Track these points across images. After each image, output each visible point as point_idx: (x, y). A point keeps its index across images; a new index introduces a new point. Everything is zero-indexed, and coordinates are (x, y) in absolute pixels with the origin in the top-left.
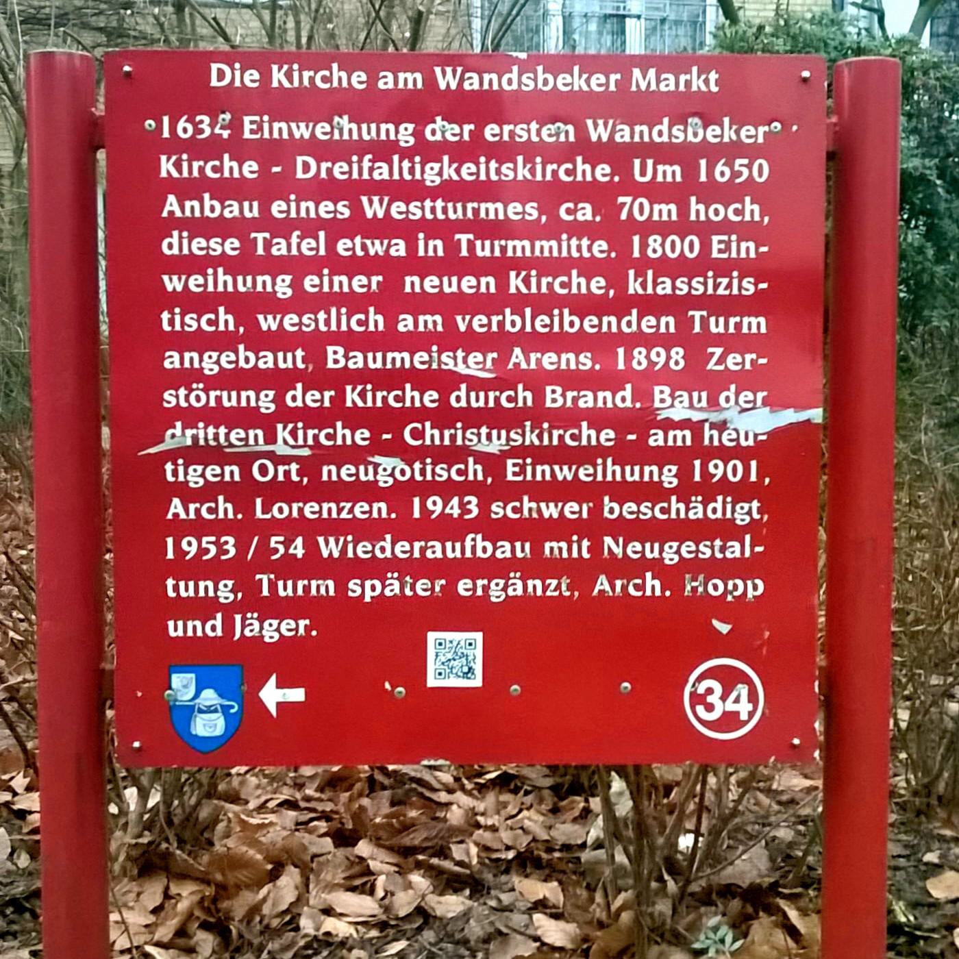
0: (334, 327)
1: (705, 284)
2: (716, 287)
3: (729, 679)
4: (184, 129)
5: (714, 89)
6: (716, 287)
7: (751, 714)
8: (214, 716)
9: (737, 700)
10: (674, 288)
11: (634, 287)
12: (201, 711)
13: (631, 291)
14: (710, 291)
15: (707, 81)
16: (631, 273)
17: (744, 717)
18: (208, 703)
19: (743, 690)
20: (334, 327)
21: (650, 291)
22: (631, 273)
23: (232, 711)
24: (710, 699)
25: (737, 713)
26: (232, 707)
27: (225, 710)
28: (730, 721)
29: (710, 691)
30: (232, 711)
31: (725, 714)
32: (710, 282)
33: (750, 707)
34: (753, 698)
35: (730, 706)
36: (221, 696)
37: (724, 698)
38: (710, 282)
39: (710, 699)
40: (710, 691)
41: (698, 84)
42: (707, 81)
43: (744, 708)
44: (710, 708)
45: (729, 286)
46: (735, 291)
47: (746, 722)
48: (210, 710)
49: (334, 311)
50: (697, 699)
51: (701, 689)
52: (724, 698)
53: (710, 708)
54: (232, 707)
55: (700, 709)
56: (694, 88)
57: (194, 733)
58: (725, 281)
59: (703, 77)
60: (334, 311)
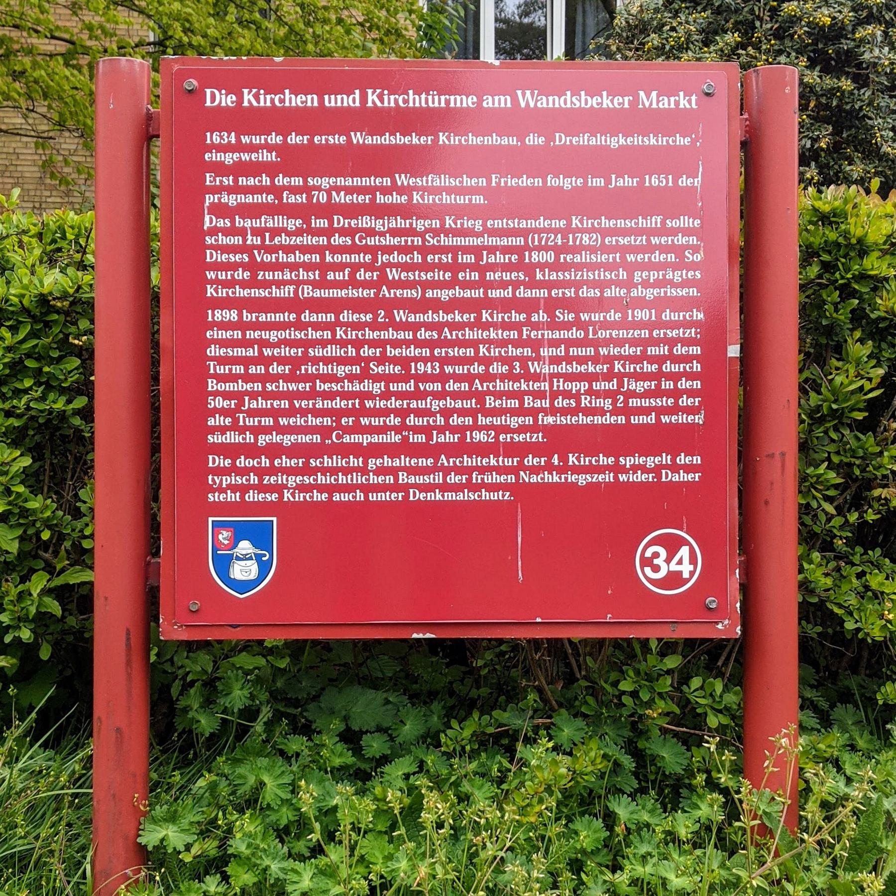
0: (355, 482)
1: (570, 275)
2: (576, 276)
3: (672, 545)
4: (216, 139)
5: (694, 106)
6: (576, 276)
7: (692, 574)
8: (249, 563)
9: (680, 562)
10: (557, 276)
11: (539, 276)
12: (238, 558)
13: (538, 278)
14: (573, 278)
15: (690, 102)
16: (538, 270)
17: (686, 575)
18: (244, 552)
19: (684, 551)
20: (355, 482)
21: (547, 278)
22: (538, 270)
23: (264, 559)
24: (656, 561)
25: (680, 573)
26: (265, 555)
27: (258, 558)
28: (674, 579)
29: (656, 555)
30: (264, 559)
31: (670, 573)
32: (573, 274)
33: (691, 568)
34: (693, 560)
35: (674, 567)
36: (255, 546)
37: (668, 561)
38: (573, 274)
39: (656, 561)
40: (656, 555)
41: (683, 103)
42: (690, 102)
43: (686, 569)
44: (656, 569)
45: (582, 275)
46: (585, 278)
47: (688, 580)
48: (246, 558)
49: (355, 474)
50: (647, 562)
51: (648, 554)
52: (668, 561)
53: (656, 569)
54: (265, 555)
55: (648, 570)
56: (681, 106)
57: (232, 577)
58: (580, 273)
59: (687, 98)
60: (355, 474)
